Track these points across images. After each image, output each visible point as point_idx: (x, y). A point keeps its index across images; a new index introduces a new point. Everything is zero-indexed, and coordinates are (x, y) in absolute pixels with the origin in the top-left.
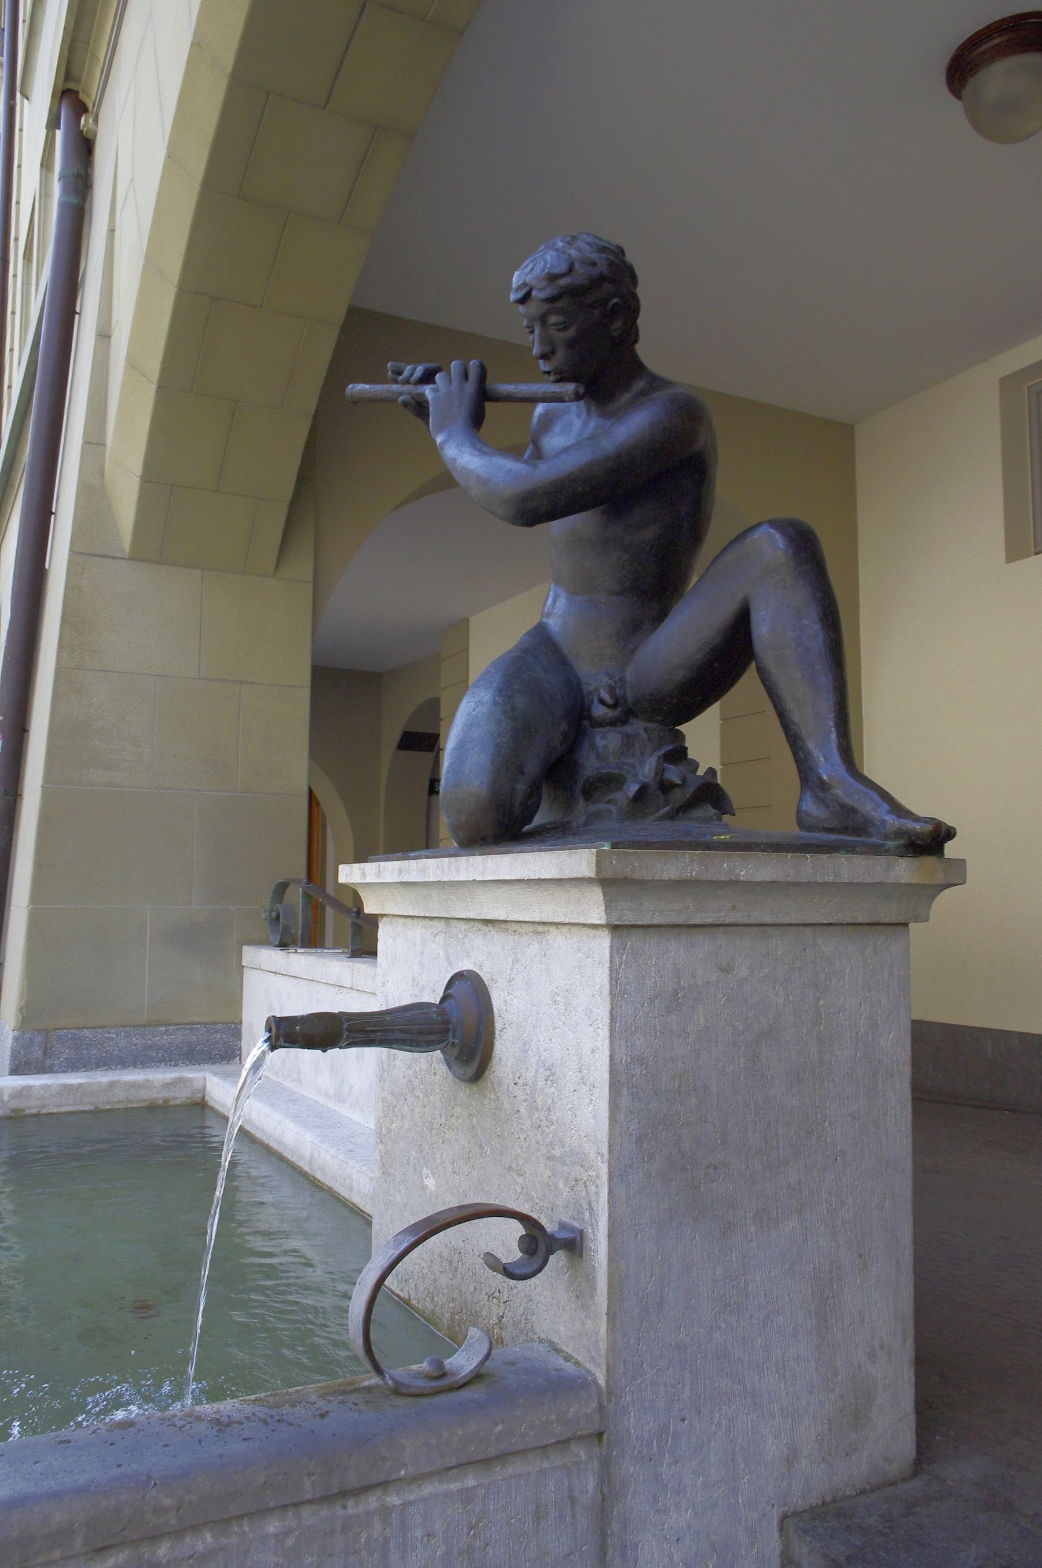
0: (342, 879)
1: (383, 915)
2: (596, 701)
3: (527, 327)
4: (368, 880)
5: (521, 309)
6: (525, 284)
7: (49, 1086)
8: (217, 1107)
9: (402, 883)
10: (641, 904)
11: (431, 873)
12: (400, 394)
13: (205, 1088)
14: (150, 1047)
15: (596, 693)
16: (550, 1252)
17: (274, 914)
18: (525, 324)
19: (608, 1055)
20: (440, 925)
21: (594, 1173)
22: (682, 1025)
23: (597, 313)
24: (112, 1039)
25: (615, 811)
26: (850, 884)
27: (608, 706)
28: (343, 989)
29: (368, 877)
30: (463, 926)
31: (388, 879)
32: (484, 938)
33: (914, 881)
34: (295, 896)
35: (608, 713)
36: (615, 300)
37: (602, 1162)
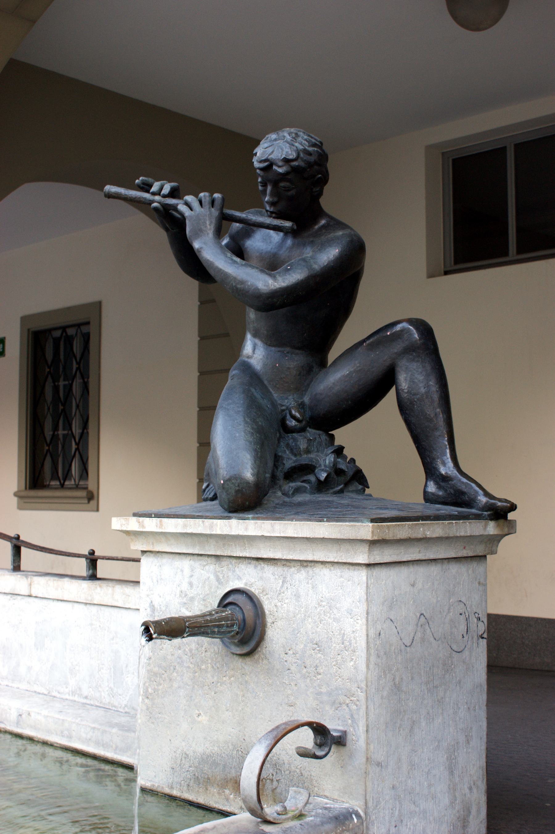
19: (366, 634)
20: (213, 559)
25: (309, 487)
26: (471, 536)
33: (496, 533)
36: (320, 176)
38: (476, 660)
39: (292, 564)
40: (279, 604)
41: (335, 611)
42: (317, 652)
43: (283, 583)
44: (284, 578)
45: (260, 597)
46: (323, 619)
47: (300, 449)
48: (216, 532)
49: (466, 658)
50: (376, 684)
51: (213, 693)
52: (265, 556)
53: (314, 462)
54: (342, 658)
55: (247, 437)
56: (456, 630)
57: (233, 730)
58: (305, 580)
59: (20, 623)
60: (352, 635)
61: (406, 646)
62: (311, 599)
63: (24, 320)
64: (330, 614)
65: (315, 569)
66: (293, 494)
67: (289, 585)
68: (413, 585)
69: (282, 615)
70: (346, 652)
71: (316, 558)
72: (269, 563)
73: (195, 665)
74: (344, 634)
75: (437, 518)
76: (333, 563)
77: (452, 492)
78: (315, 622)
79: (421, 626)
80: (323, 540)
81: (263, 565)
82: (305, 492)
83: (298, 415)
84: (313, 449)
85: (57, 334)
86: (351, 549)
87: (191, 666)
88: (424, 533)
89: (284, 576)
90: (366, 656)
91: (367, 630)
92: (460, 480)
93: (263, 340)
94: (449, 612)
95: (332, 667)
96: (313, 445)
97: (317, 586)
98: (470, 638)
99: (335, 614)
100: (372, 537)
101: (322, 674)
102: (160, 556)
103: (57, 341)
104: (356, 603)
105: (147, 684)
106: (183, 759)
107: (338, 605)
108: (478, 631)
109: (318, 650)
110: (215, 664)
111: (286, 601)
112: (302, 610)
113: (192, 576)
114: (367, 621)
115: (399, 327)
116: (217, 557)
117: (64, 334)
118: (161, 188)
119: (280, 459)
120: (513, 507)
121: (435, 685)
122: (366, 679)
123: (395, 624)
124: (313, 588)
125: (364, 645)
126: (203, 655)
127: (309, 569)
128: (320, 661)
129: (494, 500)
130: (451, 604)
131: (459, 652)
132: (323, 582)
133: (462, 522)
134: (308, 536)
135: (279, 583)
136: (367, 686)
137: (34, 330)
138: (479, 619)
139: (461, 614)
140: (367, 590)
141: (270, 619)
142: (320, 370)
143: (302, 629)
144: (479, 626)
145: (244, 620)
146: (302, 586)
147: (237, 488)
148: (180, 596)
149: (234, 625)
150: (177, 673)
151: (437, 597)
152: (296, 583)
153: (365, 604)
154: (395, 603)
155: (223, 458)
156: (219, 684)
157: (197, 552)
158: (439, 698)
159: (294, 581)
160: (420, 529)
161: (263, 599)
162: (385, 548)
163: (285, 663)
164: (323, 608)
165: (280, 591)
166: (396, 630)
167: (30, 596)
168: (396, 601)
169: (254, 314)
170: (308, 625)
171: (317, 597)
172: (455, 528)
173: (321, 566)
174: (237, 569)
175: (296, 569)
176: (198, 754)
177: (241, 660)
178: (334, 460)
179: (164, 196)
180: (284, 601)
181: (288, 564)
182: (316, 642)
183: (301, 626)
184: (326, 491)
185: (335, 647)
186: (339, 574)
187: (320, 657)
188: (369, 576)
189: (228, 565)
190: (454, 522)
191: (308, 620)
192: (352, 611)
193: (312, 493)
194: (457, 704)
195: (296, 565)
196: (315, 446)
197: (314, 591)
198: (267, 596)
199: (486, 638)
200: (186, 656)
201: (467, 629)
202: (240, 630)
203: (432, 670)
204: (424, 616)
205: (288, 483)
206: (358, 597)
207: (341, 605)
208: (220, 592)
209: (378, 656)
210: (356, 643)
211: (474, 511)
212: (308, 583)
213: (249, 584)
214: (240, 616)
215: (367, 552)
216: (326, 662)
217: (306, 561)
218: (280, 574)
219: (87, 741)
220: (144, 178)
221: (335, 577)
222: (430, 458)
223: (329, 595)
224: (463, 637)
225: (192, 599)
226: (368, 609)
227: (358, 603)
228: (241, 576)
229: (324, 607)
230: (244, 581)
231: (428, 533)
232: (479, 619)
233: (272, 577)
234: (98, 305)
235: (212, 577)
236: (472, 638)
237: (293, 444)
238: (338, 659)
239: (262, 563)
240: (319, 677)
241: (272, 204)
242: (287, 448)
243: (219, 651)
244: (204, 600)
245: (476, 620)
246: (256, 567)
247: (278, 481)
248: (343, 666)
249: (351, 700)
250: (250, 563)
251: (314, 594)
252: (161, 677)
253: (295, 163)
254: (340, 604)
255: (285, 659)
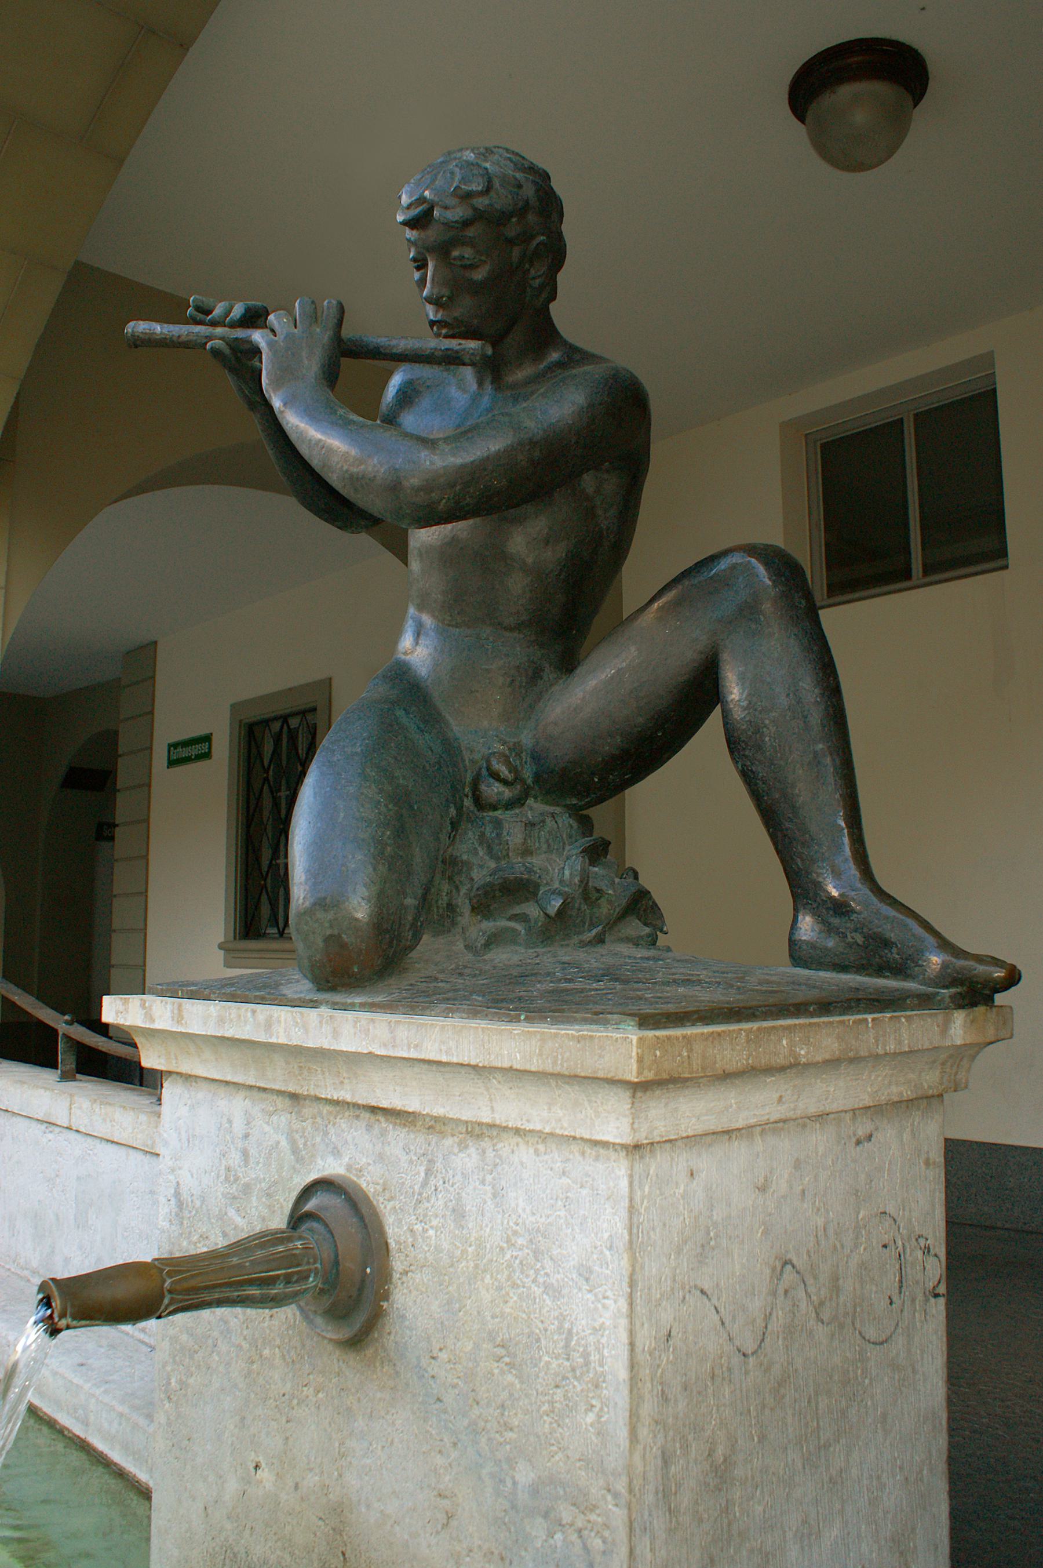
3: (414, 260)
4: (158, 1025)
5: (410, 234)
6: (422, 200)
9: (223, 1039)
10: (676, 1110)
12: (210, 338)
18: (411, 256)
21: (599, 1519)
22: (715, 1279)
23: (516, 252)
26: (911, 1052)
27: (505, 782)
28: (53, 1127)
29: (157, 1021)
30: (326, 1109)
31: (195, 1028)
37: (617, 1505)
38: (922, 1352)
40: (418, 1227)
42: (506, 1368)
43: (426, 1174)
44: (429, 1161)
45: (378, 1201)
46: (519, 1282)
48: (278, 1038)
49: (898, 1354)
50: (660, 1478)
51: (284, 1419)
53: (535, 873)
54: (566, 1397)
56: (874, 1289)
57: (321, 1523)
58: (476, 1171)
59: (57, 1176)
60: (591, 1339)
61: (744, 1355)
62: (490, 1225)
63: (235, 708)
64: (537, 1272)
66: (487, 945)
67: (441, 1182)
68: (763, 1189)
69: (426, 1258)
70: (576, 1383)
72: (398, 1121)
73: (250, 1344)
74: (570, 1331)
75: (825, 1007)
77: (860, 939)
78: (500, 1288)
79: (786, 1292)
80: (514, 1074)
81: (384, 1125)
82: (514, 942)
84: (537, 845)
85: (276, 726)
86: (586, 1103)
87: (243, 1343)
88: (792, 1052)
89: (430, 1157)
90: (628, 1407)
91: (632, 1333)
92: (878, 912)
93: (437, 614)
94: (856, 1246)
95: (541, 1417)
96: (539, 838)
98: (908, 1303)
99: (547, 1274)
100: (639, 1073)
101: (516, 1430)
103: (277, 739)
104: (602, 1252)
105: (169, 1368)
106: (227, 1561)
107: (555, 1252)
108: (927, 1280)
109: (506, 1364)
111: (434, 1222)
112: (470, 1249)
113: (246, 1136)
114: (631, 1304)
115: (723, 564)
117: (285, 727)
118: (228, 313)
119: (465, 869)
120: (1013, 978)
121: (822, 1442)
122: (629, 1468)
123: (714, 1301)
124: (495, 1195)
125: (623, 1374)
126: (266, 1325)
128: (511, 1395)
129: (966, 959)
130: (861, 1223)
131: (882, 1343)
132: (519, 1185)
133: (891, 1017)
135: (418, 1173)
136: (631, 1491)
137: (247, 721)
138: (927, 1250)
139: (885, 1246)
140: (631, 1219)
141: (399, 1263)
142: (558, 679)
143: (469, 1301)
144: (928, 1267)
145: (336, 1262)
146: (471, 1187)
147: (328, 932)
148: (227, 1179)
149: (308, 1277)
150: (218, 1353)
151: (827, 1211)
152: (456, 1178)
153: (625, 1256)
154: (712, 1243)
155: (302, 859)
156: (295, 1401)
157: (251, 1082)
158: (834, 1473)
159: (451, 1172)
160: (780, 1041)
161: (384, 1211)
162: (681, 1099)
163: (431, 1382)
164: (520, 1253)
165: (420, 1194)
166: (716, 1318)
167: (69, 1128)
168: (717, 1236)
169: (418, 562)
170: (483, 1292)
171: (505, 1222)
172: (872, 1033)
174: (332, 1130)
175: (456, 1140)
176: (255, 1560)
178: (583, 870)
179: (233, 326)
182: (502, 1340)
183: (467, 1295)
184: (563, 939)
185: (548, 1363)
186: (559, 1164)
187: (512, 1384)
188: (636, 1178)
189: (314, 1117)
190: (869, 1017)
191: (483, 1280)
192: (591, 1272)
194: (879, 1477)
196: (543, 840)
198: (392, 1203)
199: (944, 1295)
200: (236, 1320)
201: (901, 1281)
202: (326, 1287)
203: (813, 1404)
204: (793, 1267)
206: (606, 1235)
207: (564, 1252)
208: (299, 1180)
209: (664, 1398)
210: (601, 1365)
211: (911, 985)
212: (483, 1182)
213: (356, 1169)
214: (326, 1253)
215: (627, 1112)
216: (526, 1401)
220: (197, 297)
221: (549, 1172)
222: (802, 860)
223: (533, 1219)
224: (891, 1303)
225: (247, 1189)
226: (634, 1270)
227: (607, 1253)
228: (339, 1147)
229: (520, 1249)
230: (346, 1160)
231: (803, 1052)
232: (929, 1252)
233: (404, 1158)
234: (327, 684)
235: (284, 1143)
236: (913, 1300)
238: (557, 1398)
241: (435, 301)
242: (481, 844)
243: (295, 1322)
244: (269, 1195)
245: (920, 1254)
247: (459, 918)
248: (567, 1421)
249: (589, 1521)
250: (357, 1117)
252: (191, 1358)
253: (481, 202)
254: (560, 1247)
255: (432, 1373)
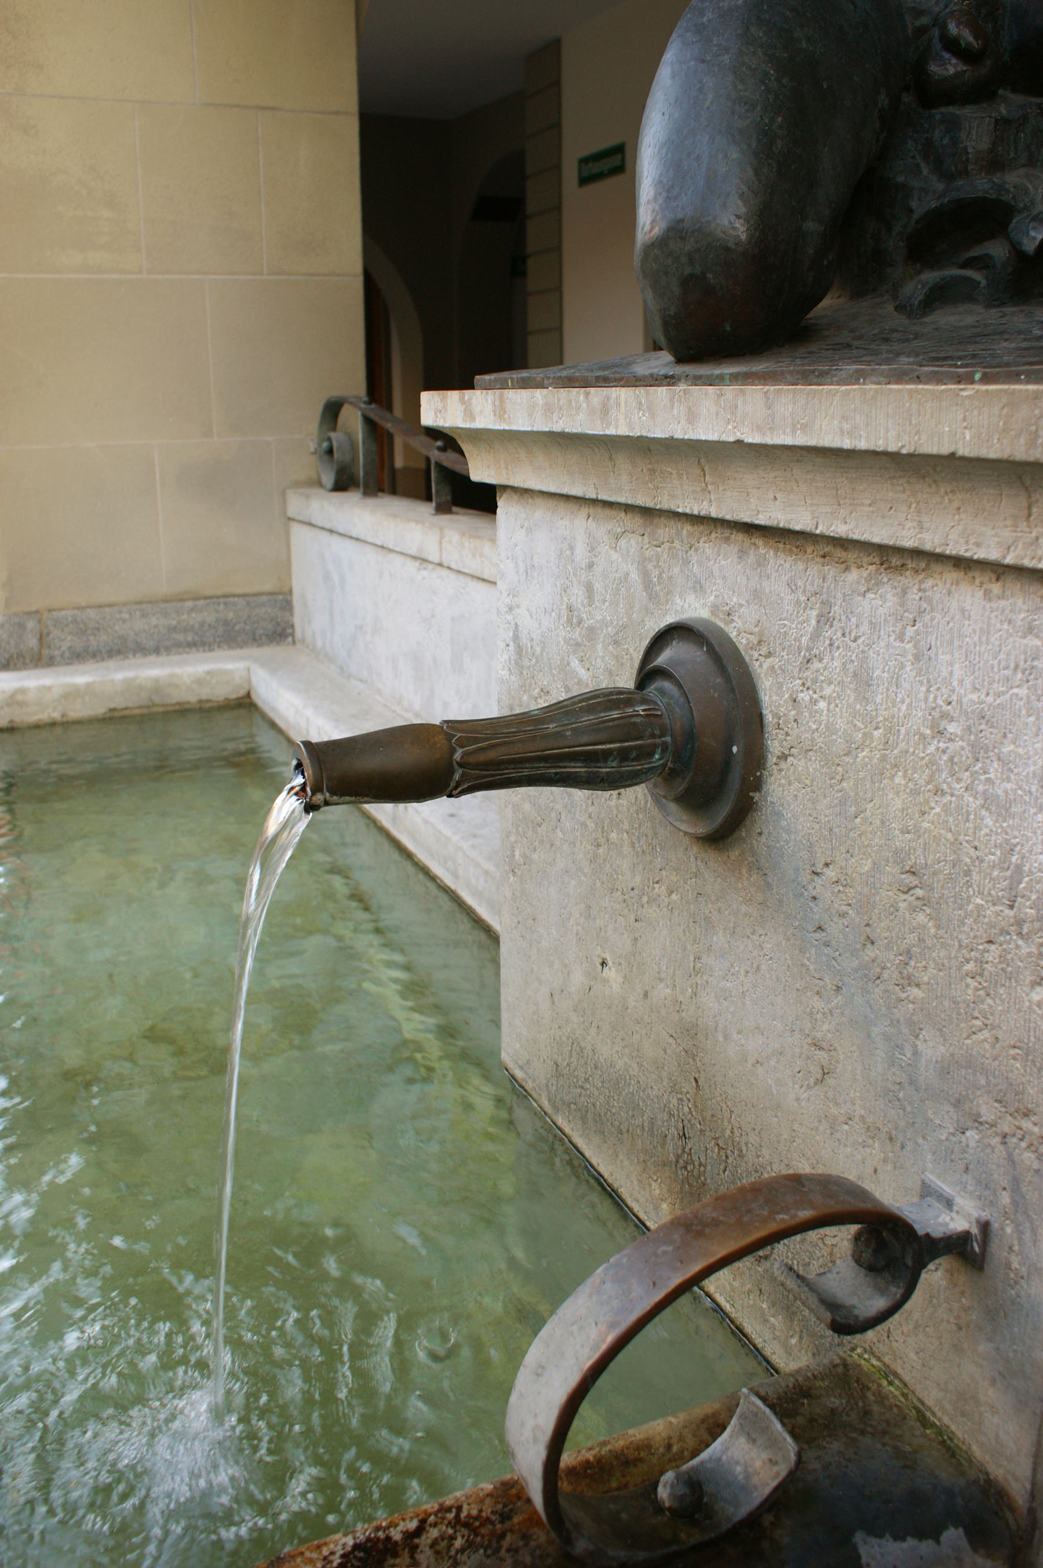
0: (427, 419)
1: (505, 488)
2: (937, 44)
4: (480, 423)
7: (49, 689)
8: (266, 709)
11: (621, 417)
13: (249, 681)
14: (175, 629)
15: (936, 32)
16: (920, 1265)
17: (325, 445)
20: (634, 521)
24: (124, 621)
25: (983, 283)
29: (477, 419)
31: (521, 424)
32: (740, 558)
34: (352, 420)
35: (965, 72)
39: (851, 556)
40: (804, 696)
41: (994, 769)
47: (967, 153)
52: (761, 520)
55: (740, 87)
62: (908, 701)
65: (929, 583)
67: (839, 634)
69: (813, 739)
70: (1020, 942)
71: (930, 542)
72: (781, 545)
74: (1019, 868)
76: (999, 570)
78: (915, 792)
81: (762, 551)
83: (967, 37)
89: (824, 596)
97: (932, 653)
102: (530, 500)
105: (512, 839)
110: (639, 840)
113: (591, 566)
116: (647, 513)
124: (917, 658)
127: (908, 580)
132: (956, 643)
134: (892, 448)
135: (808, 620)
146: (882, 644)
147: (688, 271)
152: (862, 629)
159: (854, 620)
161: (759, 670)
167: (440, 565)
173: (952, 575)
175: (865, 574)
177: (695, 849)
180: (822, 689)
181: (839, 553)
185: (979, 907)
193: (994, 301)
195: (865, 560)
197: (919, 673)
205: (919, 273)
207: (1021, 751)
212: (901, 638)
217: (900, 551)
218: (812, 589)
219: (476, 893)
221: (1005, 626)
223: (974, 697)
233: (788, 598)
235: (634, 576)
237: (945, 141)
239: (760, 542)
240: (915, 992)
246: (742, 553)
250: (727, 540)
251: (921, 683)
